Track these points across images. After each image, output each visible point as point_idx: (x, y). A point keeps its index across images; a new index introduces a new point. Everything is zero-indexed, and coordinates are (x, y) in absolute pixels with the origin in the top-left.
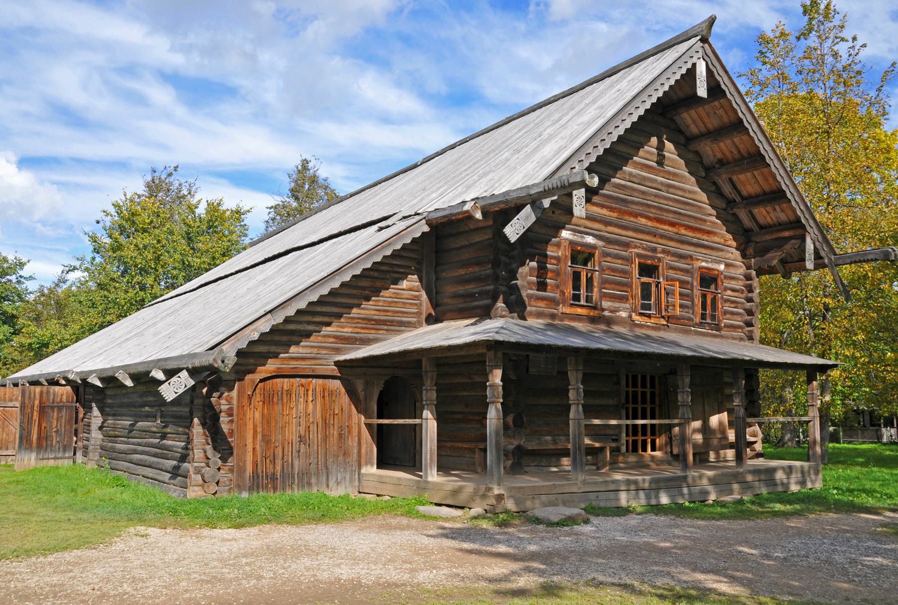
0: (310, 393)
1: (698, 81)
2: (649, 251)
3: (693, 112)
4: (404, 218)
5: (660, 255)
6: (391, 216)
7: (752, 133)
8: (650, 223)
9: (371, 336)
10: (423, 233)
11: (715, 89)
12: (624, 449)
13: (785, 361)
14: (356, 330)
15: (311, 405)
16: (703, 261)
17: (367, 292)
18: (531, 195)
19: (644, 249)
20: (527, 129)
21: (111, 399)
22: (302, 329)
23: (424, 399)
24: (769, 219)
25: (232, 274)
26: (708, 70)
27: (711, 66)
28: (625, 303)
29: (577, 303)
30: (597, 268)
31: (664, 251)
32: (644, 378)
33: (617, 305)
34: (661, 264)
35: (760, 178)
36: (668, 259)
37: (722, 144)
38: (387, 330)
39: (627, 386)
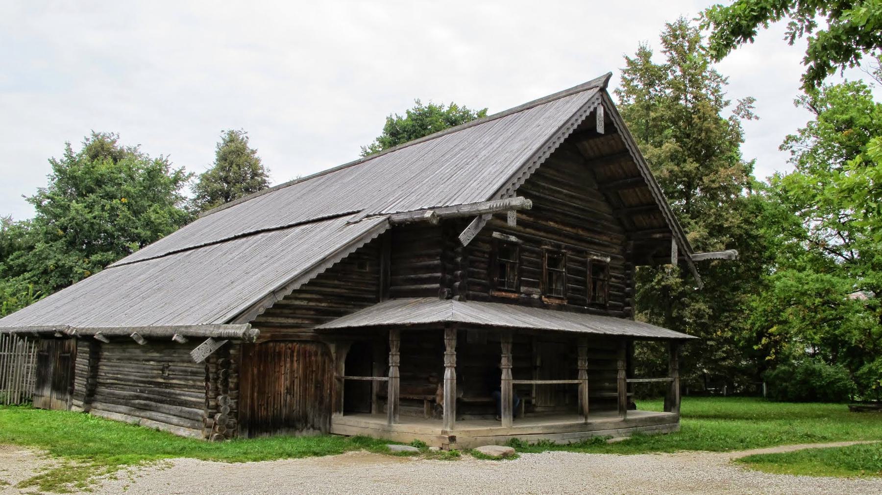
0: (295, 354)
1: (598, 122)
3: (591, 141)
4: (368, 216)
5: (564, 251)
6: (358, 212)
7: (635, 161)
9: (342, 310)
11: (609, 125)
13: (656, 336)
14: (330, 305)
15: (295, 365)
16: (595, 255)
19: (552, 246)
21: (108, 352)
23: (390, 361)
25: (201, 246)
27: (607, 110)
29: (502, 288)
30: (517, 262)
31: (566, 248)
33: (531, 289)
35: (639, 193)
36: (569, 254)
38: (354, 305)
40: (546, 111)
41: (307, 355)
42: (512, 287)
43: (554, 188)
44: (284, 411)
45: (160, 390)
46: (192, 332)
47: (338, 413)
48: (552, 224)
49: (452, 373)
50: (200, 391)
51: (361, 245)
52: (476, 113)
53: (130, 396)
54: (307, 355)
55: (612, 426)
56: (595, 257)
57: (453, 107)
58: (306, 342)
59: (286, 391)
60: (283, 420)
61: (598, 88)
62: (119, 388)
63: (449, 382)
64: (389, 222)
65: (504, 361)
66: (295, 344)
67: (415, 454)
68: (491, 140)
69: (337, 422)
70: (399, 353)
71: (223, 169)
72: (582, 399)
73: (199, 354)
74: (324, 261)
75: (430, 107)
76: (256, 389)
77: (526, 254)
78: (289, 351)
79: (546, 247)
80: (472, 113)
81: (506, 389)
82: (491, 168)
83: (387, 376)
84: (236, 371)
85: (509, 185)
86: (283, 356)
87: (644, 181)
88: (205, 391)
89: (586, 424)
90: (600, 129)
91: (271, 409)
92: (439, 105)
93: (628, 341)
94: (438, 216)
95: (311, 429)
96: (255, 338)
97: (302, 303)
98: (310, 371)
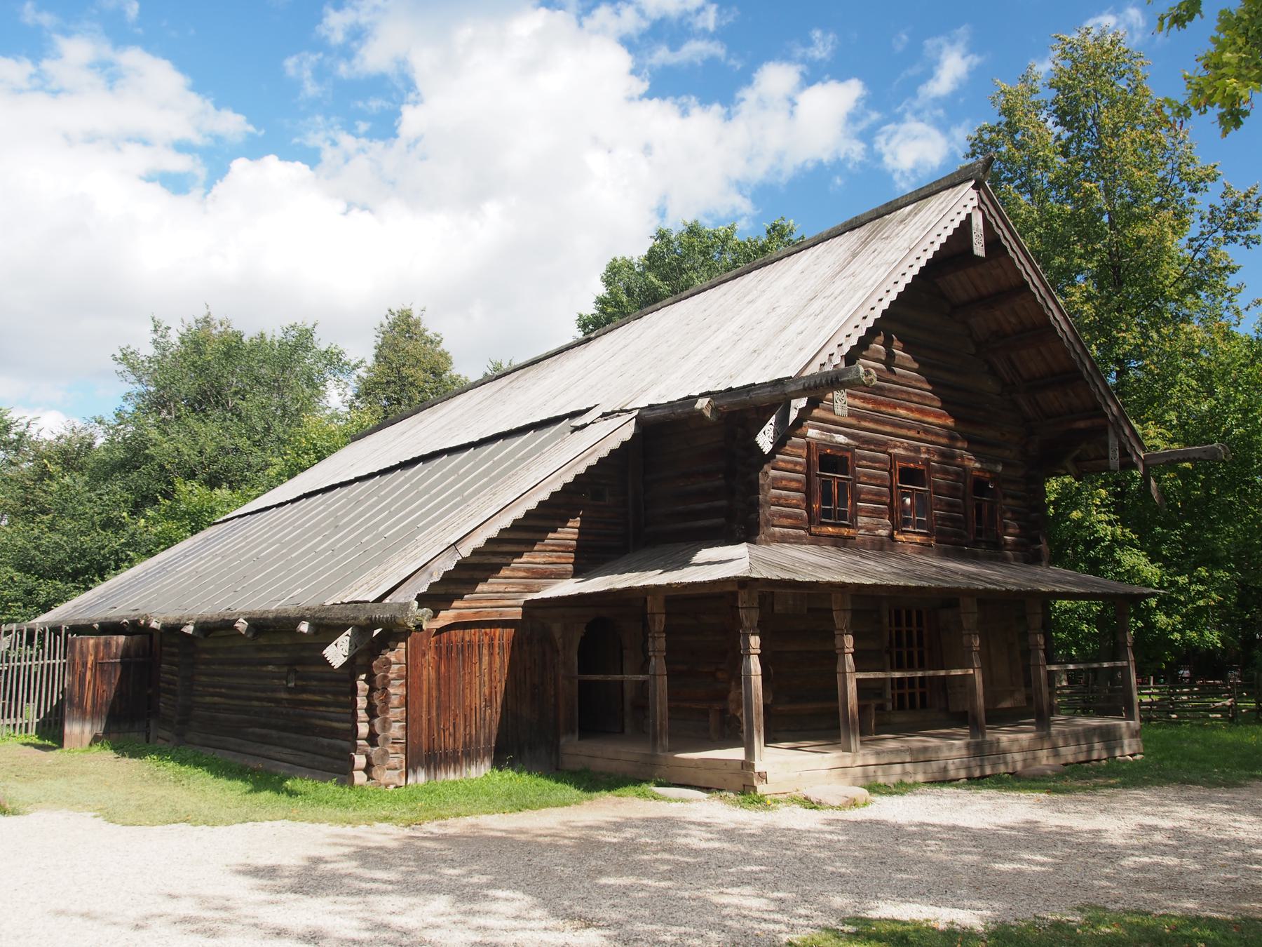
2: (911, 451)
4: (605, 415)
6: (589, 410)
8: (911, 415)
11: (992, 242)
12: (889, 706)
18: (785, 394)
19: (905, 448)
22: (486, 561)
26: (986, 223)
27: (988, 217)
32: (909, 613)
39: (890, 625)
90: (979, 250)
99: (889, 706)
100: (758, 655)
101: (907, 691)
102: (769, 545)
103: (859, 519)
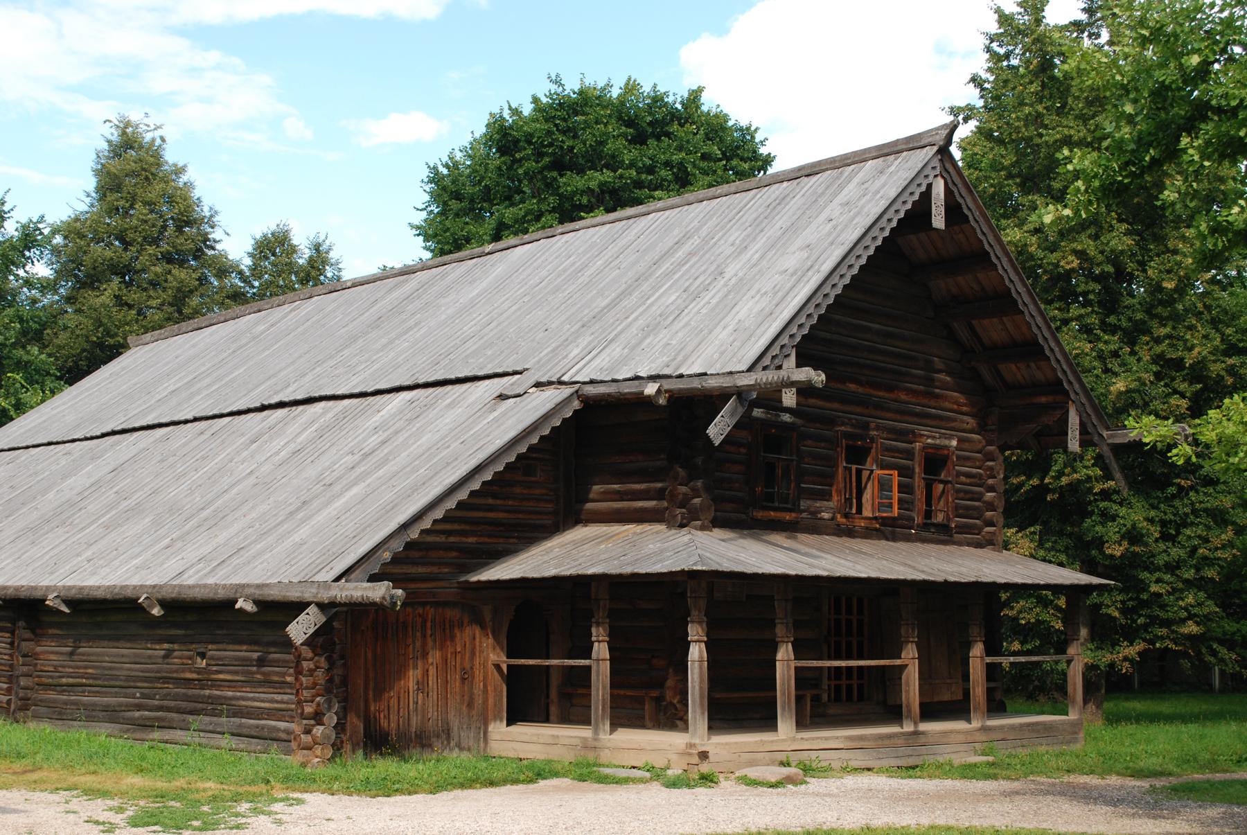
0: (429, 624)
4: (538, 385)
7: (1001, 271)
10: (576, 411)
11: (953, 210)
12: (825, 697)
16: (928, 437)
17: (495, 488)
19: (853, 426)
20: (687, 248)
24: (1020, 377)
26: (948, 191)
27: (950, 185)
28: (828, 501)
29: (770, 504)
30: (795, 458)
34: (874, 445)
37: (960, 279)
38: (517, 538)
40: (841, 188)
41: (447, 626)
42: (787, 503)
43: (855, 321)
44: (414, 720)
45: (190, 692)
46: (275, 594)
47: (498, 722)
48: (852, 387)
49: (700, 651)
50: (279, 690)
51: (535, 440)
52: (679, 100)
53: (120, 705)
54: (447, 626)
55: (961, 738)
56: (929, 441)
57: (631, 87)
58: (445, 604)
59: (416, 687)
60: (413, 735)
61: (935, 148)
62: (93, 692)
63: (697, 664)
64: (579, 397)
65: (474, 579)
66: (428, 607)
67: (642, 781)
68: (744, 240)
69: (498, 737)
70: (608, 621)
71: (113, 211)
72: (908, 692)
73: (300, 629)
74: (478, 469)
75: (581, 92)
76: (371, 685)
77: (809, 442)
78: (419, 620)
79: (843, 428)
80: (670, 99)
81: (784, 675)
82: (750, 304)
83: (590, 658)
84: (342, 657)
85: (785, 340)
86: (410, 629)
87: (1017, 305)
88: (294, 692)
89: (916, 733)
90: (938, 222)
91: (393, 717)
92: (601, 84)
93: (987, 592)
94: (666, 391)
95: (457, 749)
96: (399, 603)
97: (438, 539)
98: (452, 654)
99: (825, 697)
100: (705, 642)
101: (844, 682)
102: (711, 531)
103: (802, 503)
